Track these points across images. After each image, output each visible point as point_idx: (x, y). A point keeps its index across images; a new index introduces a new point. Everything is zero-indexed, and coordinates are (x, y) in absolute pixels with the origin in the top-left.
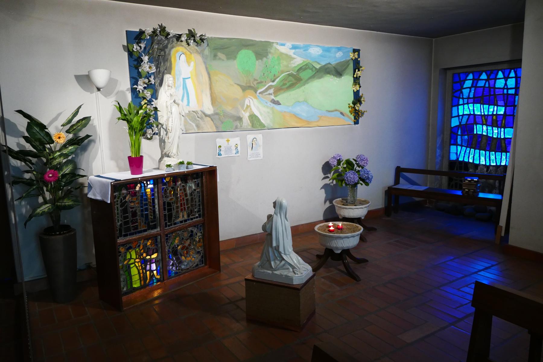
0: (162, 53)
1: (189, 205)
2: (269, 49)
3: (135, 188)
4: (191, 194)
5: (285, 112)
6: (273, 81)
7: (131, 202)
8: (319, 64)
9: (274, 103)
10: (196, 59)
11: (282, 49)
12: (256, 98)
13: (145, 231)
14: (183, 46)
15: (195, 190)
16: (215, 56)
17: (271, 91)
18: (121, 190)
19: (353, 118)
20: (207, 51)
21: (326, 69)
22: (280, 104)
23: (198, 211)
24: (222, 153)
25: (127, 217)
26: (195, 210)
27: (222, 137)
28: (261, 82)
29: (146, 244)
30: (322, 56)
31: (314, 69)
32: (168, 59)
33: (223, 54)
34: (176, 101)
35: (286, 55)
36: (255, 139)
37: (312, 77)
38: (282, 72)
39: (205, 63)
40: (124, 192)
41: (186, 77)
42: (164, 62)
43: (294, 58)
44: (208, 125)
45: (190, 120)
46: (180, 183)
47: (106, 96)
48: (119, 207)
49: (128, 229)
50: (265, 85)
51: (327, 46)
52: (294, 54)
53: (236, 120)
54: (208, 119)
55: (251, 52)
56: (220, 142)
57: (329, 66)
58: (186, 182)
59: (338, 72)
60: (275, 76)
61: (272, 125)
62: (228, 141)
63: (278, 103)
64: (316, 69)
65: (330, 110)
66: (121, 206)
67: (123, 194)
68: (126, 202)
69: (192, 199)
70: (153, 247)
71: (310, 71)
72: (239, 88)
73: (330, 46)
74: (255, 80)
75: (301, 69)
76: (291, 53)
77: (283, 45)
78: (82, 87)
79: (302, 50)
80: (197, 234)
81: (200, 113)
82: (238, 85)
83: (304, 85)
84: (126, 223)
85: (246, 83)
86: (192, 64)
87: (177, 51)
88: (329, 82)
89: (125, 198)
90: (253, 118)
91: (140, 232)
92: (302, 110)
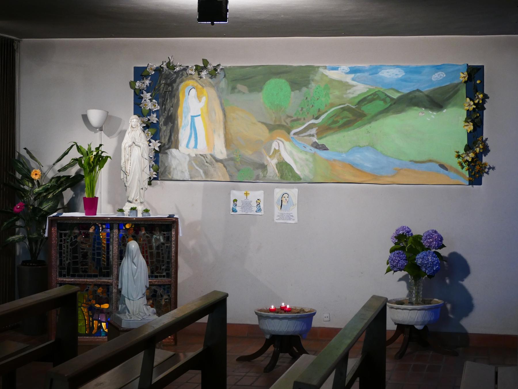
0: (170, 88)
1: (154, 260)
2: (311, 76)
3: (89, 230)
4: (158, 248)
5: (334, 160)
6: (317, 118)
7: (82, 243)
8: (397, 91)
9: (316, 148)
10: (210, 93)
11: (333, 75)
12: (288, 140)
13: (95, 276)
14: (194, 79)
15: (163, 244)
16: (234, 89)
17: (314, 131)
18: (73, 229)
19: (467, 174)
20: (223, 84)
21: (412, 99)
22: (327, 149)
23: (166, 270)
24: (237, 208)
25: (76, 257)
26: (163, 267)
27: (239, 189)
28: (298, 120)
29: (96, 291)
30: (402, 80)
31: (388, 100)
32: (175, 95)
33: (245, 85)
34: (136, 143)
35: (340, 82)
36: (286, 195)
37: (385, 112)
38: (332, 105)
39: (220, 98)
40: (77, 231)
41: (195, 115)
42: (171, 99)
43: (353, 86)
44: (220, 173)
45: (197, 165)
46: (143, 232)
47: (108, 136)
48: (69, 246)
49: (76, 270)
50: (304, 124)
51: (413, 65)
52: (353, 79)
53: (257, 168)
54: (221, 165)
55: (284, 81)
56: (235, 194)
57: (417, 94)
58: (152, 234)
59: (436, 101)
60: (319, 110)
61: (311, 177)
62: (247, 194)
63: (323, 148)
64: (392, 99)
65: (418, 159)
66: (71, 245)
67: (75, 233)
68: (76, 242)
69: (158, 253)
70: (105, 296)
71: (382, 103)
72: (264, 128)
73: (420, 65)
74: (289, 117)
75: (364, 100)
76: (349, 79)
77: (336, 69)
78: (89, 129)
79: (366, 74)
80: (162, 296)
81: (209, 157)
82: (263, 123)
83: (370, 123)
84: (75, 263)
85: (275, 121)
86: (204, 99)
87: (187, 85)
88: (419, 118)
89: (76, 237)
90: (283, 166)
91: (90, 276)
92: (365, 159)
